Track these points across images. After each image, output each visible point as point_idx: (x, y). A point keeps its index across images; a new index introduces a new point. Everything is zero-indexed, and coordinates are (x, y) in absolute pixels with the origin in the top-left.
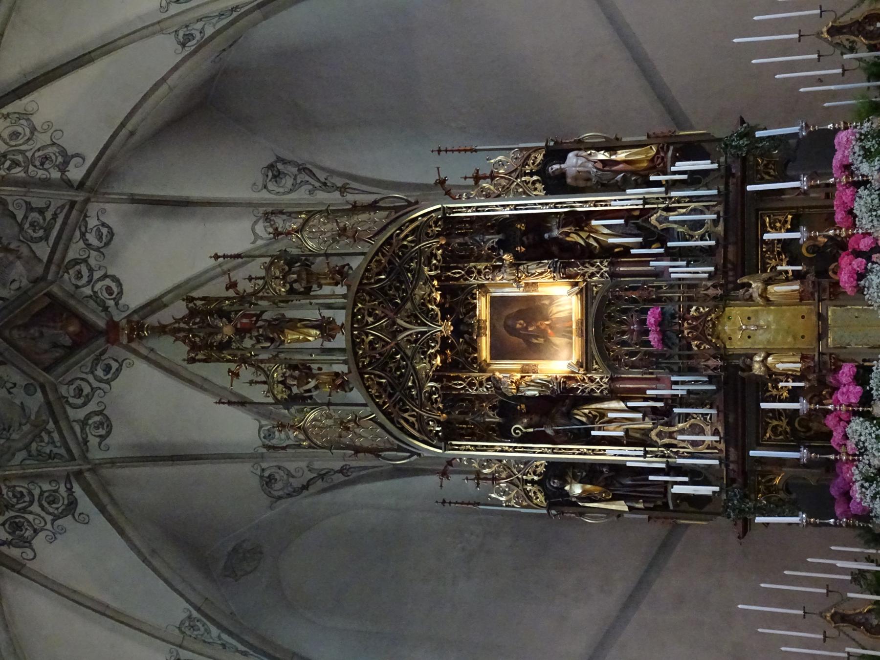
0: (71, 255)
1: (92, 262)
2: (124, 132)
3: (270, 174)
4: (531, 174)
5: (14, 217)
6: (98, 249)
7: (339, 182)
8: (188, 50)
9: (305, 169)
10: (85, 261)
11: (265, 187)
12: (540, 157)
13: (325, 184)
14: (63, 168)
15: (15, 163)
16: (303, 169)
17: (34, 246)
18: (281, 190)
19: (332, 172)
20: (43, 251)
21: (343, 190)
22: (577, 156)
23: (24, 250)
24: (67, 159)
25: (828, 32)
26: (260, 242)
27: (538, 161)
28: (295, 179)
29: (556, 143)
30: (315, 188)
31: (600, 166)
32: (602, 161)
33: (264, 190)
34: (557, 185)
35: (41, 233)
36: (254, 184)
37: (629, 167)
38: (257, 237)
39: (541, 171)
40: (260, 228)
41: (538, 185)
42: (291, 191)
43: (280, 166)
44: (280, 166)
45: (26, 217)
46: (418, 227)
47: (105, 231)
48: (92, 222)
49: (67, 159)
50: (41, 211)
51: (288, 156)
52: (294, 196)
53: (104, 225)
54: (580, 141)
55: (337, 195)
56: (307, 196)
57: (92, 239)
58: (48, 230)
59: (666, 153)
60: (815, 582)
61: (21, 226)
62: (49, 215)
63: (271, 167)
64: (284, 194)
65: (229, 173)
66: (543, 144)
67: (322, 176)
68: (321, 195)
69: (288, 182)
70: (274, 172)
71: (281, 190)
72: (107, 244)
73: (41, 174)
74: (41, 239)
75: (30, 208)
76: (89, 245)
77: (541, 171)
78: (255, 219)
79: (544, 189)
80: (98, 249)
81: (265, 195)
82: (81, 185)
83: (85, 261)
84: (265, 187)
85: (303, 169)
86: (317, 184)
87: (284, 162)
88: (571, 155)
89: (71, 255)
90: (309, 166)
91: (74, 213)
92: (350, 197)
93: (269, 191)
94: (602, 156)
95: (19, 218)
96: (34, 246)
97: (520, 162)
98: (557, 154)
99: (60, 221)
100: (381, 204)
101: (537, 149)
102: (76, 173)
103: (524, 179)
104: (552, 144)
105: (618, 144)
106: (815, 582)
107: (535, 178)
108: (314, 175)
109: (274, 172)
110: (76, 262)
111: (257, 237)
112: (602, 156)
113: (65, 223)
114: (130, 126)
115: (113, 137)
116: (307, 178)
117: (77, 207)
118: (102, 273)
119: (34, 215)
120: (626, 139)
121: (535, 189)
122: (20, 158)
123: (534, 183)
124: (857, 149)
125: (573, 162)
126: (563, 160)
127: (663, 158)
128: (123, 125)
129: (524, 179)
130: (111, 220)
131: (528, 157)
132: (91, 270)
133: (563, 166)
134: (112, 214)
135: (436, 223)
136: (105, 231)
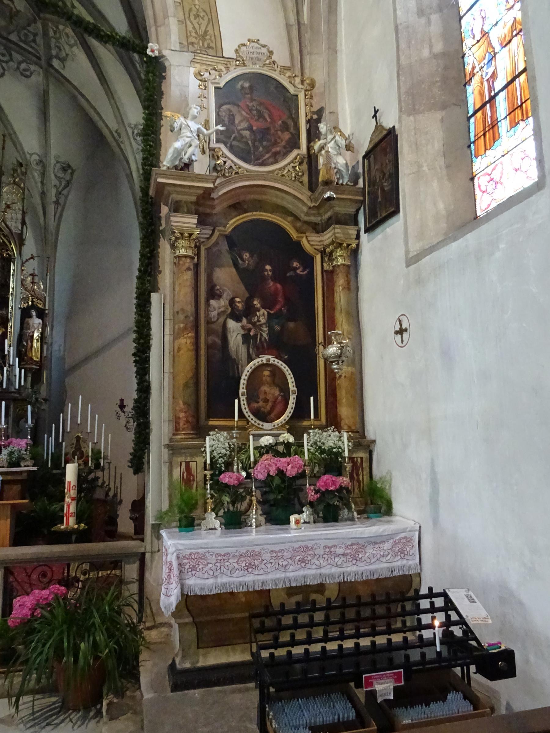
0: (14, 54)
1: (11, 63)
2: (76, 93)
3: (64, 165)
4: (32, 302)
5: (29, 25)
6: (18, 68)
7: (61, 201)
8: (114, 133)
9: (68, 184)
10: (11, 60)
11: (58, 162)
12: (40, 306)
13: (60, 193)
14: (57, 57)
15: (55, 32)
16: (68, 183)
17: (15, 33)
18: (56, 171)
19: (66, 197)
20: (13, 37)
21: (57, 203)
22: (39, 324)
23: (12, 28)
24: (63, 60)
25: (78, 436)
26: (28, 156)
27: (39, 305)
28: (62, 178)
29: (47, 314)
30: (57, 189)
31: (31, 334)
32: (33, 336)
33: (55, 162)
34: (25, 314)
35: (23, 38)
36: (59, 156)
37: (29, 347)
38: (31, 155)
39: (33, 307)
40: (35, 157)
41: (27, 304)
42: (56, 176)
43: (70, 171)
44: (70, 171)
45: (29, 31)
46: (6, 245)
47: (28, 73)
48: (32, 67)
49: (63, 60)
50: (34, 41)
51: (75, 176)
52: (53, 176)
53: (32, 73)
54: (46, 326)
55: (54, 199)
56: (53, 184)
57: (23, 66)
58: (25, 42)
59: (35, 365)
60: (93, 426)
61: (24, 28)
62: (33, 44)
63: (69, 166)
64: (54, 172)
65: (63, 144)
66: (47, 308)
67: (65, 192)
68: (53, 192)
69: (61, 175)
70: (66, 168)
71: (56, 171)
72: (22, 74)
73: (53, 45)
74: (20, 38)
75: (35, 35)
76: (20, 63)
77: (33, 307)
78: (40, 155)
79: (24, 308)
80: (18, 68)
81: (53, 162)
82: (51, 66)
83: (11, 60)
84: (58, 162)
85: (68, 183)
86: (60, 189)
87: (72, 174)
88: (40, 321)
89: (14, 54)
90: (70, 185)
91: (35, 59)
92: (53, 206)
93: (55, 165)
94: (36, 335)
95: (29, 28)
96: (15, 33)
97: (39, 297)
98: (41, 314)
99: (30, 49)
100: (25, 227)
101: (44, 305)
102: (56, 63)
103: (30, 298)
104: (47, 312)
105: (43, 344)
106: (93, 426)
107: (30, 303)
108: (66, 188)
109: (66, 168)
110: (10, 55)
111: (31, 155)
112: (36, 335)
113: (30, 53)
114: (80, 97)
115: (75, 87)
116: (63, 184)
117: (38, 61)
118: (6, 68)
119: (31, 38)
120: (45, 347)
121: (24, 303)
122: (58, 35)
123: (28, 303)
124: (15, 449)
125: (36, 321)
126: (38, 316)
127: (32, 363)
128: (81, 93)
129: (30, 298)
130: (33, 77)
131: (41, 300)
132: (7, 62)
133: (35, 317)
134: (38, 78)
135: (8, 254)
136: (28, 73)
